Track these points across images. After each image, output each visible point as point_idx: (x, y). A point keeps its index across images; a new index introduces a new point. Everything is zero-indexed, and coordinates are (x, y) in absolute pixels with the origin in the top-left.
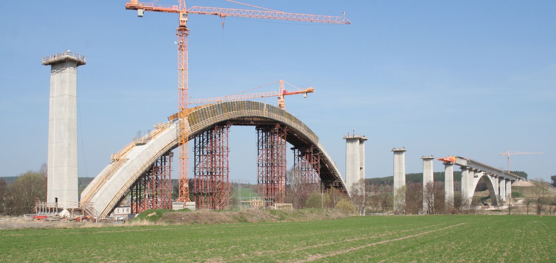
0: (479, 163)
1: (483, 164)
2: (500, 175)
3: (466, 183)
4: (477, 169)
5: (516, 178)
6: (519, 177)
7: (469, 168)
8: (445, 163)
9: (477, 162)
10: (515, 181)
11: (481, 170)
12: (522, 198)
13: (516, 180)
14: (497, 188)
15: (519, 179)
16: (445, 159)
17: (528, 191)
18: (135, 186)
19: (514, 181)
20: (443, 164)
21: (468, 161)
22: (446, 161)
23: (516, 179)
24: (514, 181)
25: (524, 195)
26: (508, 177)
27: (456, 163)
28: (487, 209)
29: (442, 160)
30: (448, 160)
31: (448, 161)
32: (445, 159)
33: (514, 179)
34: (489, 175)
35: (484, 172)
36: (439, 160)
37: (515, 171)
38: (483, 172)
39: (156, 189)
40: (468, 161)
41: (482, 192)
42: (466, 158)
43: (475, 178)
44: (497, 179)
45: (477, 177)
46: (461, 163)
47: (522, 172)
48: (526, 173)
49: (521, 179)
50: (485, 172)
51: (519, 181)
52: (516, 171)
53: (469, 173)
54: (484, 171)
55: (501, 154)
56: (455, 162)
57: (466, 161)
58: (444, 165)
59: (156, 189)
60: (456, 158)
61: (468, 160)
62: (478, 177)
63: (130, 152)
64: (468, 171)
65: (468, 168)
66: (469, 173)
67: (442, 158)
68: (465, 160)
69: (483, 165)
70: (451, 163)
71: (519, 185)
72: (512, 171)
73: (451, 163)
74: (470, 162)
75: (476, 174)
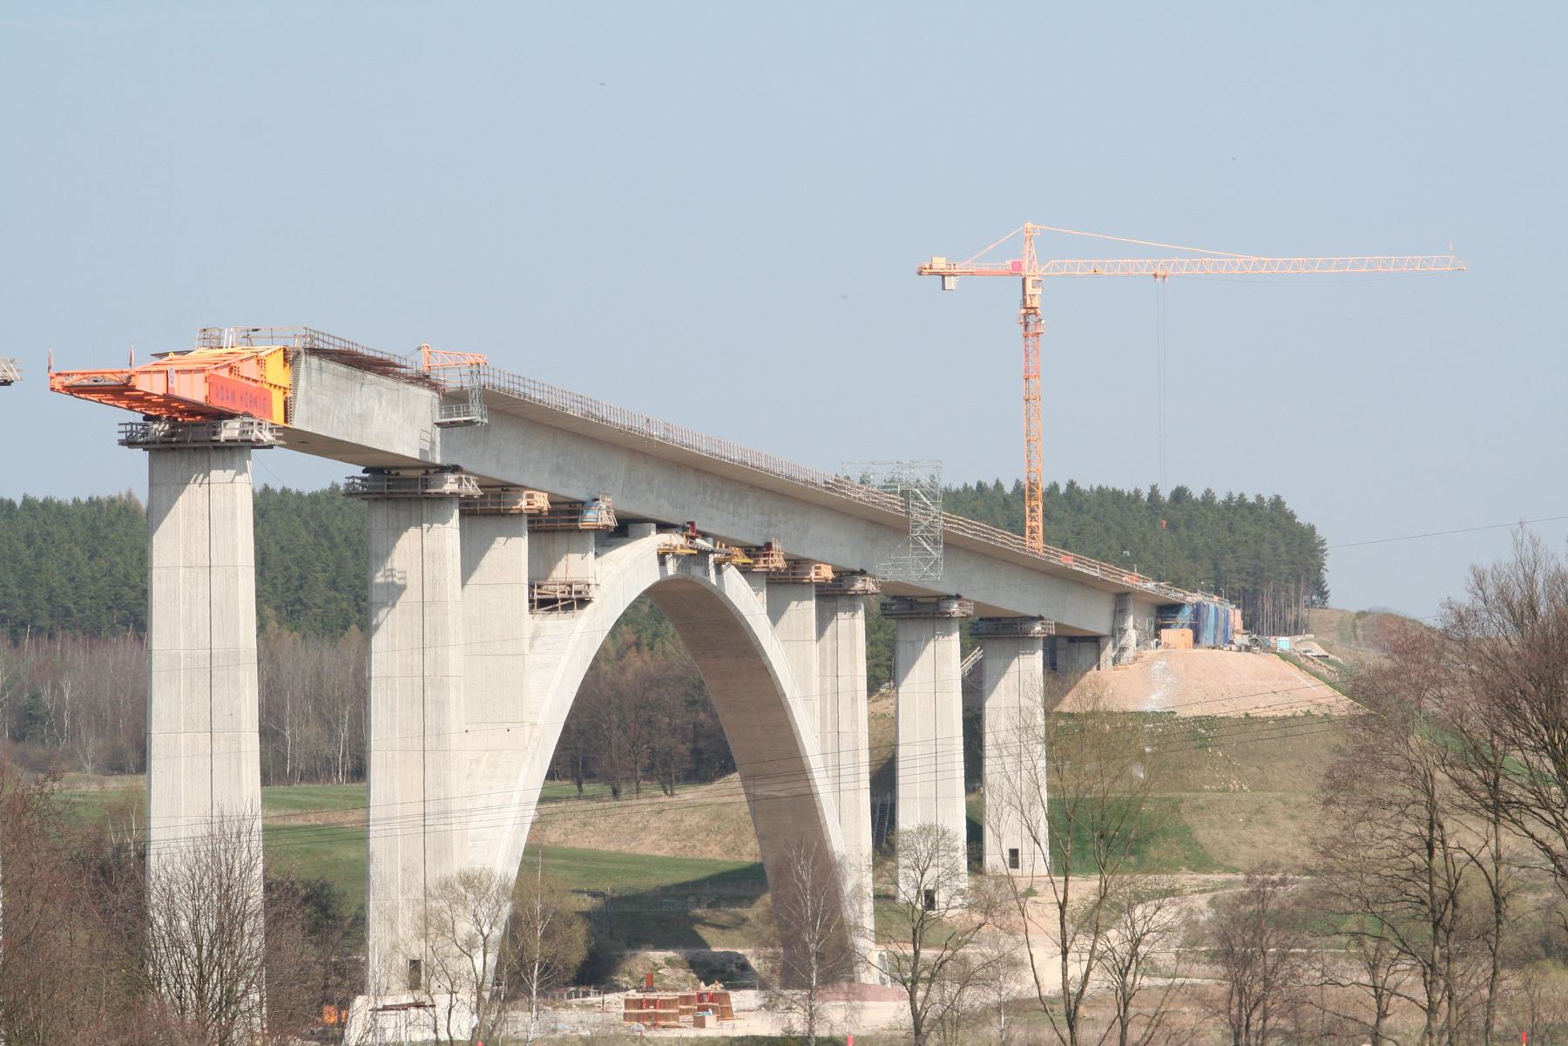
0: (601, 424)
1: (657, 433)
2: (892, 576)
3: (427, 690)
4: (576, 492)
5: (1122, 600)
6: (1150, 585)
7: (472, 489)
8: (159, 428)
9: (575, 411)
10: (1109, 652)
11: (633, 508)
12: (1186, 879)
13: (1117, 632)
14: (845, 759)
15: (1165, 613)
16: (143, 384)
17: (1262, 785)
18: (1325, 649)
19: (1094, 641)
20: (130, 443)
21: (454, 399)
22: (169, 400)
23: (1119, 612)
24: (1095, 641)
25: (1207, 834)
26: (1010, 598)
27: (297, 424)
28: (700, 1023)
29: (121, 392)
30: (194, 390)
31: (193, 409)
32: (152, 385)
33: (1094, 619)
34: (745, 570)
35: (675, 540)
36: (153, 355)
37: (1165, 494)
38: (654, 541)
39: (620, 663)
40: (454, 399)
41: (688, 794)
42: (419, 364)
43: (554, 622)
44: (852, 627)
45: (577, 601)
46: (364, 419)
47: (1239, 510)
48: (1303, 519)
49: (1186, 615)
50: (689, 530)
51: (1150, 653)
52: (1180, 494)
53: (468, 568)
54: (663, 527)
55: (940, 263)
56: (278, 417)
57: (425, 399)
58: (141, 456)
59: (620, 663)
60: (290, 358)
61: (452, 382)
62: (583, 603)
63: (1002, 855)
64: (447, 534)
65: (450, 485)
66: (470, 563)
67: (110, 367)
68: (423, 380)
69: (648, 439)
70: (230, 431)
71: (1154, 702)
72: (1127, 488)
73: (230, 431)
74: (476, 413)
75: (575, 566)
